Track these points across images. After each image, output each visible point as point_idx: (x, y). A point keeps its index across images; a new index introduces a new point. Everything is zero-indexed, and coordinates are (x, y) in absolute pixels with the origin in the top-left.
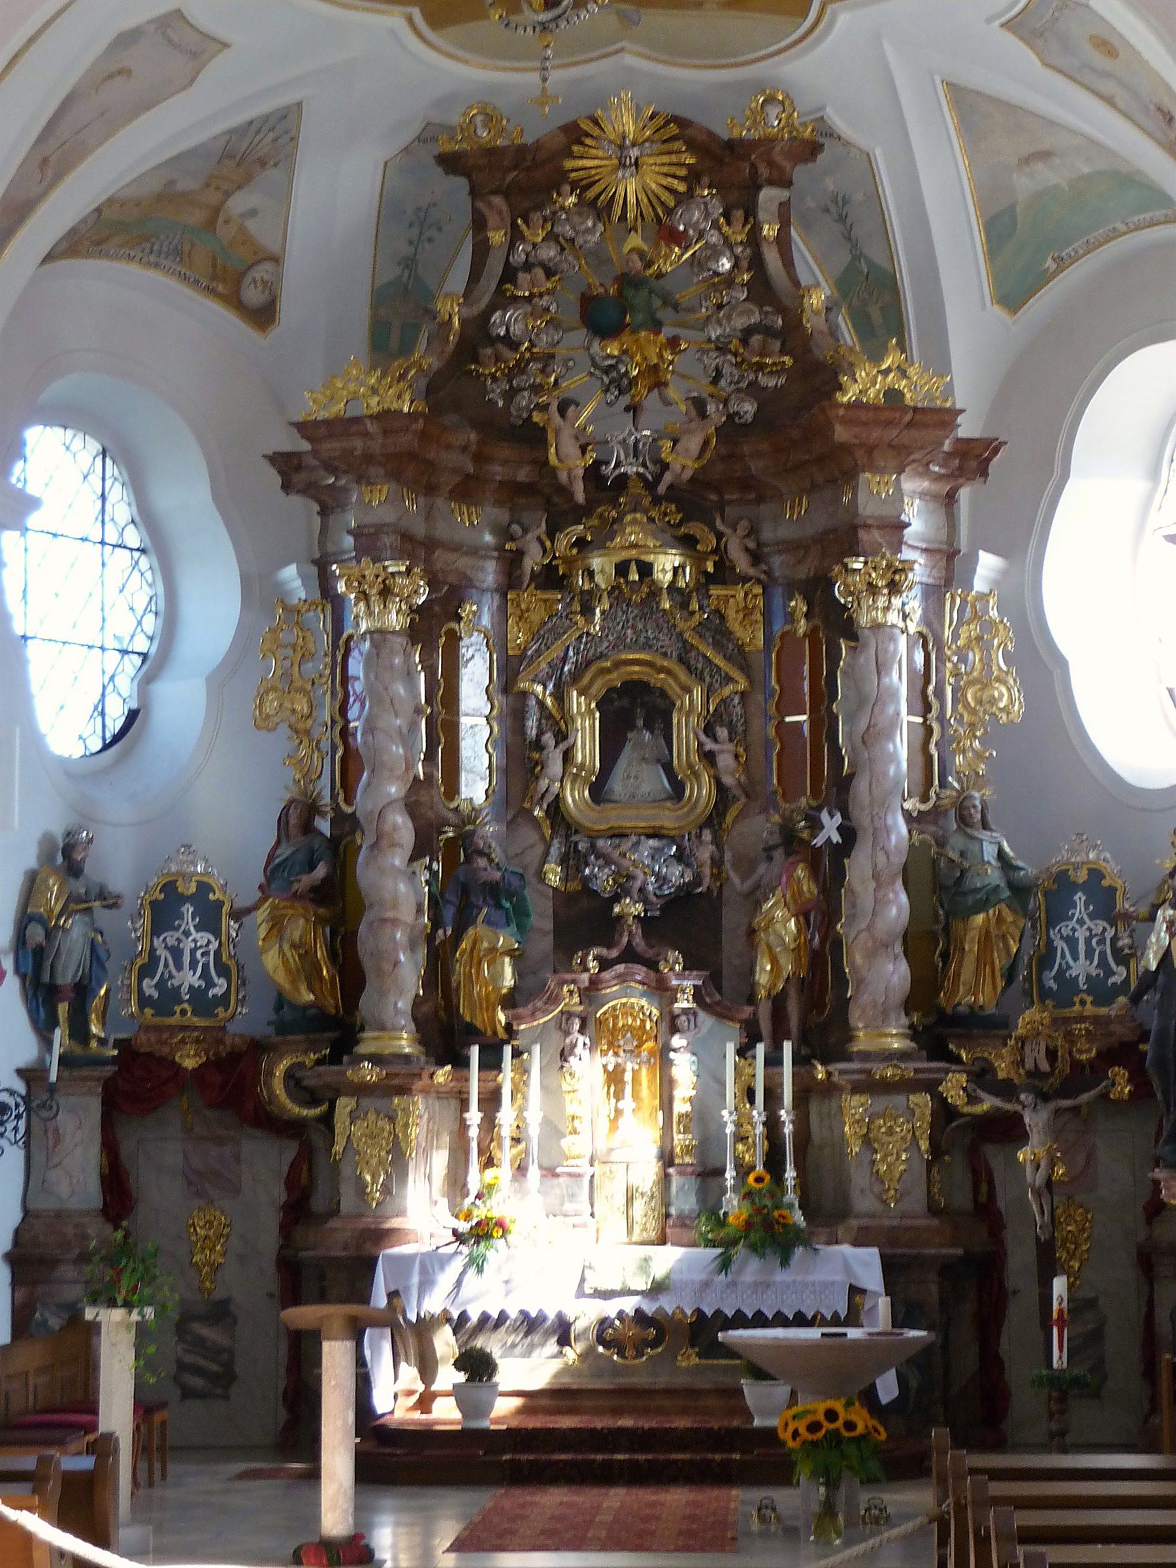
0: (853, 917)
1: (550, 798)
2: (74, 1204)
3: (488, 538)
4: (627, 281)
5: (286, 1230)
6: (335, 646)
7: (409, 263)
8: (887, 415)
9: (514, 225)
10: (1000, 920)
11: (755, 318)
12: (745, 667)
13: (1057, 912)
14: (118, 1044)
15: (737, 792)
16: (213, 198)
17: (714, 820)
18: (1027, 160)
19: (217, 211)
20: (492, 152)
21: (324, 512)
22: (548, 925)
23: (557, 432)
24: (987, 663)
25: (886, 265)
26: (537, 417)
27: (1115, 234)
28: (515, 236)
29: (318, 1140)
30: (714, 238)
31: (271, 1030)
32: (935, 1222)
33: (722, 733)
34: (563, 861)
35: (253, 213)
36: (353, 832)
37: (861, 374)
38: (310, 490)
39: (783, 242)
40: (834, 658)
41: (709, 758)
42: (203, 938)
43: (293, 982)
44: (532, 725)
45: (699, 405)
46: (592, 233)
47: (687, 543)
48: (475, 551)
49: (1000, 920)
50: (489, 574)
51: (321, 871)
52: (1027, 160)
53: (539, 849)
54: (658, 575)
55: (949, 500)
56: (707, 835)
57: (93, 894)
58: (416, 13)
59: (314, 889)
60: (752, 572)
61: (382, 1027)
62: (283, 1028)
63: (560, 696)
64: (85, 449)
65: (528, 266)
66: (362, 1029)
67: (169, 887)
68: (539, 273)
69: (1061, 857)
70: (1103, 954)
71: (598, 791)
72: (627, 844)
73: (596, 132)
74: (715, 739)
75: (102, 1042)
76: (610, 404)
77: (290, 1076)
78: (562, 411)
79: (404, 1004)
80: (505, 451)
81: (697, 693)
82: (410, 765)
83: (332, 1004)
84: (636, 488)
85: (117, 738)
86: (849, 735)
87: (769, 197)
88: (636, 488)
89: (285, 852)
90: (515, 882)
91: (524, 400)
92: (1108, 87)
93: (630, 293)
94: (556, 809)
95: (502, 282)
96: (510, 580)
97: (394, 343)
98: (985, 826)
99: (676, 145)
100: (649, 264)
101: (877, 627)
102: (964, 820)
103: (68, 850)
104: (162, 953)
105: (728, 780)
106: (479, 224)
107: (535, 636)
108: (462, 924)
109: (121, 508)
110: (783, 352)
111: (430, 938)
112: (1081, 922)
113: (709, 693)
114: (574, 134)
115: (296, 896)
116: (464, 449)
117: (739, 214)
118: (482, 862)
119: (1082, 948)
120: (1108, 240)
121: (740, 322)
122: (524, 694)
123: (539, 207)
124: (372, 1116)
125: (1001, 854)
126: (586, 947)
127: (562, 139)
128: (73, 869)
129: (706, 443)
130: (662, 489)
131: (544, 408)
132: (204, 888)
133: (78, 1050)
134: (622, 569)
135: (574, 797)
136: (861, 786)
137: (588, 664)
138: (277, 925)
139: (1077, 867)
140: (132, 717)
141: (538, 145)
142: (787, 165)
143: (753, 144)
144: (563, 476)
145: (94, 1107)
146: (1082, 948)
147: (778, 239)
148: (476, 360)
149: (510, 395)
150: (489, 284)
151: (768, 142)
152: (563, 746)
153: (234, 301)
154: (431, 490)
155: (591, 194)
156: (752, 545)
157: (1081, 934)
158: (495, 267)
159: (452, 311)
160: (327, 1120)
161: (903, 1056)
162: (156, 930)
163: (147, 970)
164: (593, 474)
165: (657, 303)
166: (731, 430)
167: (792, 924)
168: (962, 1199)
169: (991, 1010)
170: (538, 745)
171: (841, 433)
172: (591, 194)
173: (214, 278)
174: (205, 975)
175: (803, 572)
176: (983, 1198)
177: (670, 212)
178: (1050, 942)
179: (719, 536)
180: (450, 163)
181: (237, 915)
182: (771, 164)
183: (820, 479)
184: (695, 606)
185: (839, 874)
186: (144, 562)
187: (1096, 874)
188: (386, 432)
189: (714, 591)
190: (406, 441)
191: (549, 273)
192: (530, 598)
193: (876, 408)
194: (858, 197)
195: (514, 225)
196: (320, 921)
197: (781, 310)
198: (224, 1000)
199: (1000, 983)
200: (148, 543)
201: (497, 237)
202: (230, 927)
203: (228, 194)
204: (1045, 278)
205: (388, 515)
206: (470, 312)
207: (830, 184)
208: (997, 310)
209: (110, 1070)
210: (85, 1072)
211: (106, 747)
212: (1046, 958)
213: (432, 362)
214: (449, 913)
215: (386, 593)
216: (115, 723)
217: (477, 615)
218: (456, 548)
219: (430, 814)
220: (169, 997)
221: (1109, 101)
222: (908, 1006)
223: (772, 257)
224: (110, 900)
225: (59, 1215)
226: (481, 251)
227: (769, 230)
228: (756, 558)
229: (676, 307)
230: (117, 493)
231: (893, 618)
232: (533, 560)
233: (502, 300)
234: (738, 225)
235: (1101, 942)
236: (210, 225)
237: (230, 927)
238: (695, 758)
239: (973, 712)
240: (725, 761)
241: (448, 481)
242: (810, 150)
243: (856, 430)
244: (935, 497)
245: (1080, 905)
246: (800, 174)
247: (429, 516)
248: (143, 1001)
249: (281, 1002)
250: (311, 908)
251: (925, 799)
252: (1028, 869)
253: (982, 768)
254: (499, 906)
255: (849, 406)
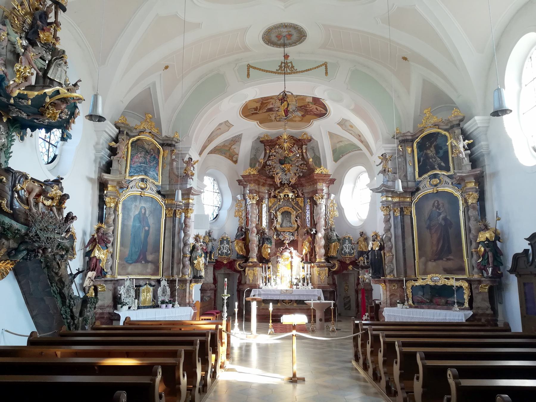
0: (317, 243)
1: (275, 226)
2: (209, 282)
3: (267, 191)
4: (285, 157)
5: (238, 286)
6: (245, 206)
7: (255, 155)
8: (322, 175)
9: (270, 150)
10: (336, 243)
11: (302, 163)
12: (301, 209)
13: (344, 243)
14: (215, 260)
15: (300, 226)
16: (230, 146)
17: (297, 230)
18: (338, 142)
19: (230, 148)
20: (267, 140)
21: (244, 188)
22: (274, 244)
23: (276, 177)
24: (334, 209)
25: (319, 156)
26: (273, 175)
27: (350, 152)
28: (270, 151)
29: (243, 273)
30: (297, 152)
31: (236, 258)
32: (329, 286)
33: (298, 218)
34: (276, 235)
35: (235, 148)
36: (248, 231)
37: (318, 170)
38: (242, 185)
39: (306, 152)
40: (314, 208)
41: (296, 221)
42: (227, 245)
43: (240, 252)
44: (272, 216)
45: (295, 174)
46: (280, 151)
47: (293, 192)
48: (265, 193)
49: (336, 243)
50: (267, 196)
51: (243, 236)
52: (338, 142)
53: (273, 233)
54: (290, 196)
55: (328, 187)
56: (296, 232)
57: (213, 239)
58: (258, 122)
59: (243, 239)
60: (302, 196)
61: (252, 258)
62: (238, 258)
63: (276, 213)
64: (212, 179)
65: (272, 155)
66: (249, 258)
67: (223, 238)
68: (273, 156)
69: (344, 235)
70: (350, 249)
71: (281, 226)
72: (285, 233)
73: (281, 138)
74: (297, 219)
75: (213, 260)
76: (283, 174)
77: (239, 265)
78: (277, 174)
79: (255, 255)
80: (269, 180)
81: (295, 212)
82: (256, 222)
83: (245, 255)
84: (286, 185)
85: (215, 218)
86: (316, 218)
87: (304, 147)
88: (286, 185)
89: (238, 234)
90: (270, 238)
91: (271, 173)
92: (351, 132)
93: (286, 159)
94: (275, 228)
95: (268, 157)
96: (269, 197)
97: (253, 165)
98: (334, 231)
99: (292, 140)
100: (288, 155)
101: (320, 203)
102: (331, 230)
103: (209, 233)
104: (222, 247)
105: (299, 224)
106: (265, 150)
107: (273, 204)
108: (263, 244)
109: (216, 187)
110: (306, 167)
111: (259, 245)
112: (347, 244)
113: (296, 212)
114: (278, 138)
115: (240, 240)
116: (264, 179)
117: (300, 149)
118: (266, 235)
119: (347, 248)
120: (349, 153)
121: (300, 163)
122: (271, 212)
123: (273, 148)
124: (251, 270)
125: (336, 235)
126: (280, 247)
127: (276, 139)
128: (210, 236)
129: (296, 179)
130: (290, 185)
131: (274, 174)
132: (227, 238)
133: (210, 260)
134: (285, 196)
135: (278, 227)
136: (318, 225)
137: (280, 208)
138: (237, 243)
139: (347, 237)
140: (217, 215)
141: (273, 140)
142: (307, 142)
143: (302, 139)
144: (277, 183)
145: (212, 268)
146: (347, 248)
147: (305, 152)
148: (265, 168)
149: (269, 172)
150: (267, 158)
151: (305, 139)
152: (276, 219)
153: (232, 160)
154: (259, 185)
155: (280, 146)
156: (302, 193)
157: (347, 246)
158: (267, 155)
159: (262, 161)
160: (244, 271)
161: (324, 262)
162: (221, 245)
163: (219, 250)
164: (281, 183)
165: (289, 160)
166: (299, 177)
167: (308, 244)
168: (331, 282)
169: (335, 256)
170: (273, 219)
171: (315, 177)
172: (280, 146)
173: (229, 157)
174: (227, 251)
175: (309, 196)
176: (334, 282)
177: (291, 148)
178: (343, 247)
179: (298, 191)
180: (262, 142)
181: (231, 242)
182: (304, 142)
183: (311, 184)
184: (294, 201)
185: (315, 238)
186: (219, 194)
187: (349, 238)
188: (254, 177)
189: (297, 199)
190: (256, 178)
191: (275, 156)
192: (272, 200)
193: (320, 174)
194: (315, 147)
195: (270, 150)
196: (243, 243)
197: (306, 161)
198: (230, 254)
199: (337, 253)
200: (219, 192)
201: (268, 152)
202: (230, 244)
203: (232, 146)
204: (340, 158)
205: (254, 188)
206: (264, 161)
207: (312, 145)
208: (334, 162)
209: (214, 264)
210: (211, 264)
211: (214, 219)
212: (342, 249)
213: (259, 168)
214: (261, 242)
215: (253, 198)
216: (215, 216)
217: (265, 202)
218: (262, 193)
219: (259, 229)
220: (222, 253)
221: (351, 134)
222: (324, 255)
223: (304, 154)
224: (215, 240)
225: (207, 283)
226: (266, 153)
227: (304, 151)
228: (303, 194)
229: (292, 161)
230: (215, 185)
231: (322, 202)
232: (272, 194)
233: (268, 160)
234: (300, 150)
235: (350, 247)
236: (229, 150)
237: (230, 244)
238: (294, 221)
239: (332, 215)
240: (299, 222)
241: (261, 184)
242: (310, 140)
243: (317, 177)
244: (327, 187)
245: (347, 242)
246: (308, 144)
247: (259, 188)
248: (219, 254)
249: (238, 254)
250: (242, 241)
251: (326, 227)
252: (340, 237)
253: (333, 223)
254: (268, 241)
255: (316, 174)
